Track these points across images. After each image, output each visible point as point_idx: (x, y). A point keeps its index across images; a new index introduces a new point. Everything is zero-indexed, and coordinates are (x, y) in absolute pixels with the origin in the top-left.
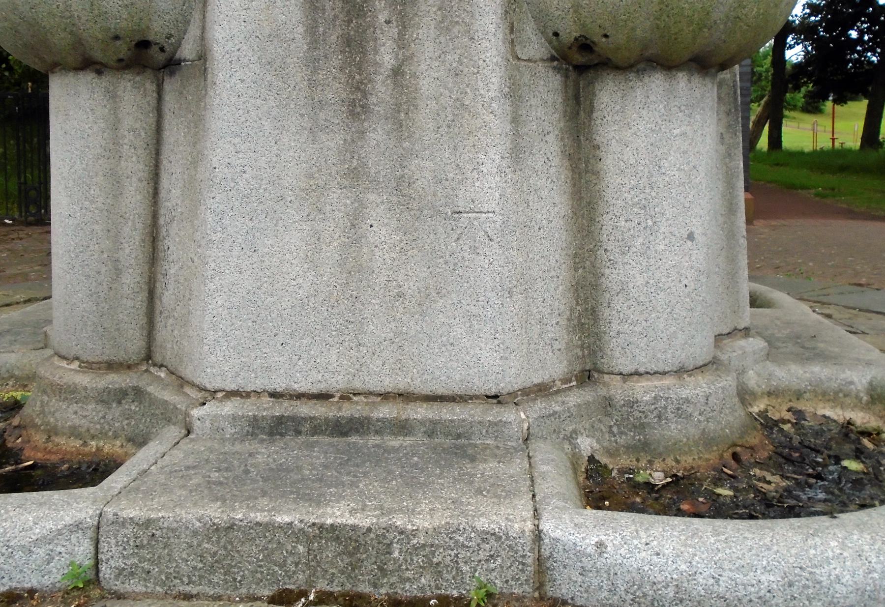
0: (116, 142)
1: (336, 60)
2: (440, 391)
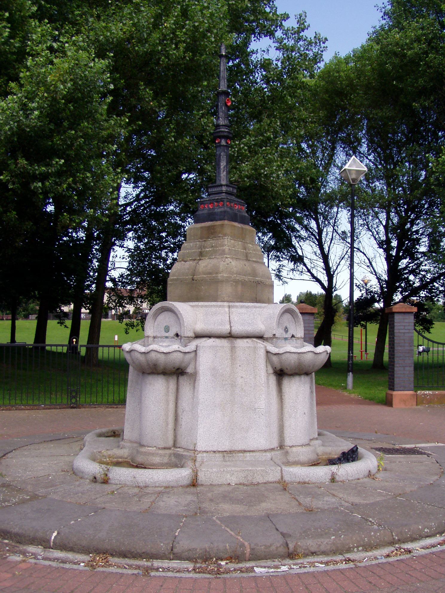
0: (168, 392)
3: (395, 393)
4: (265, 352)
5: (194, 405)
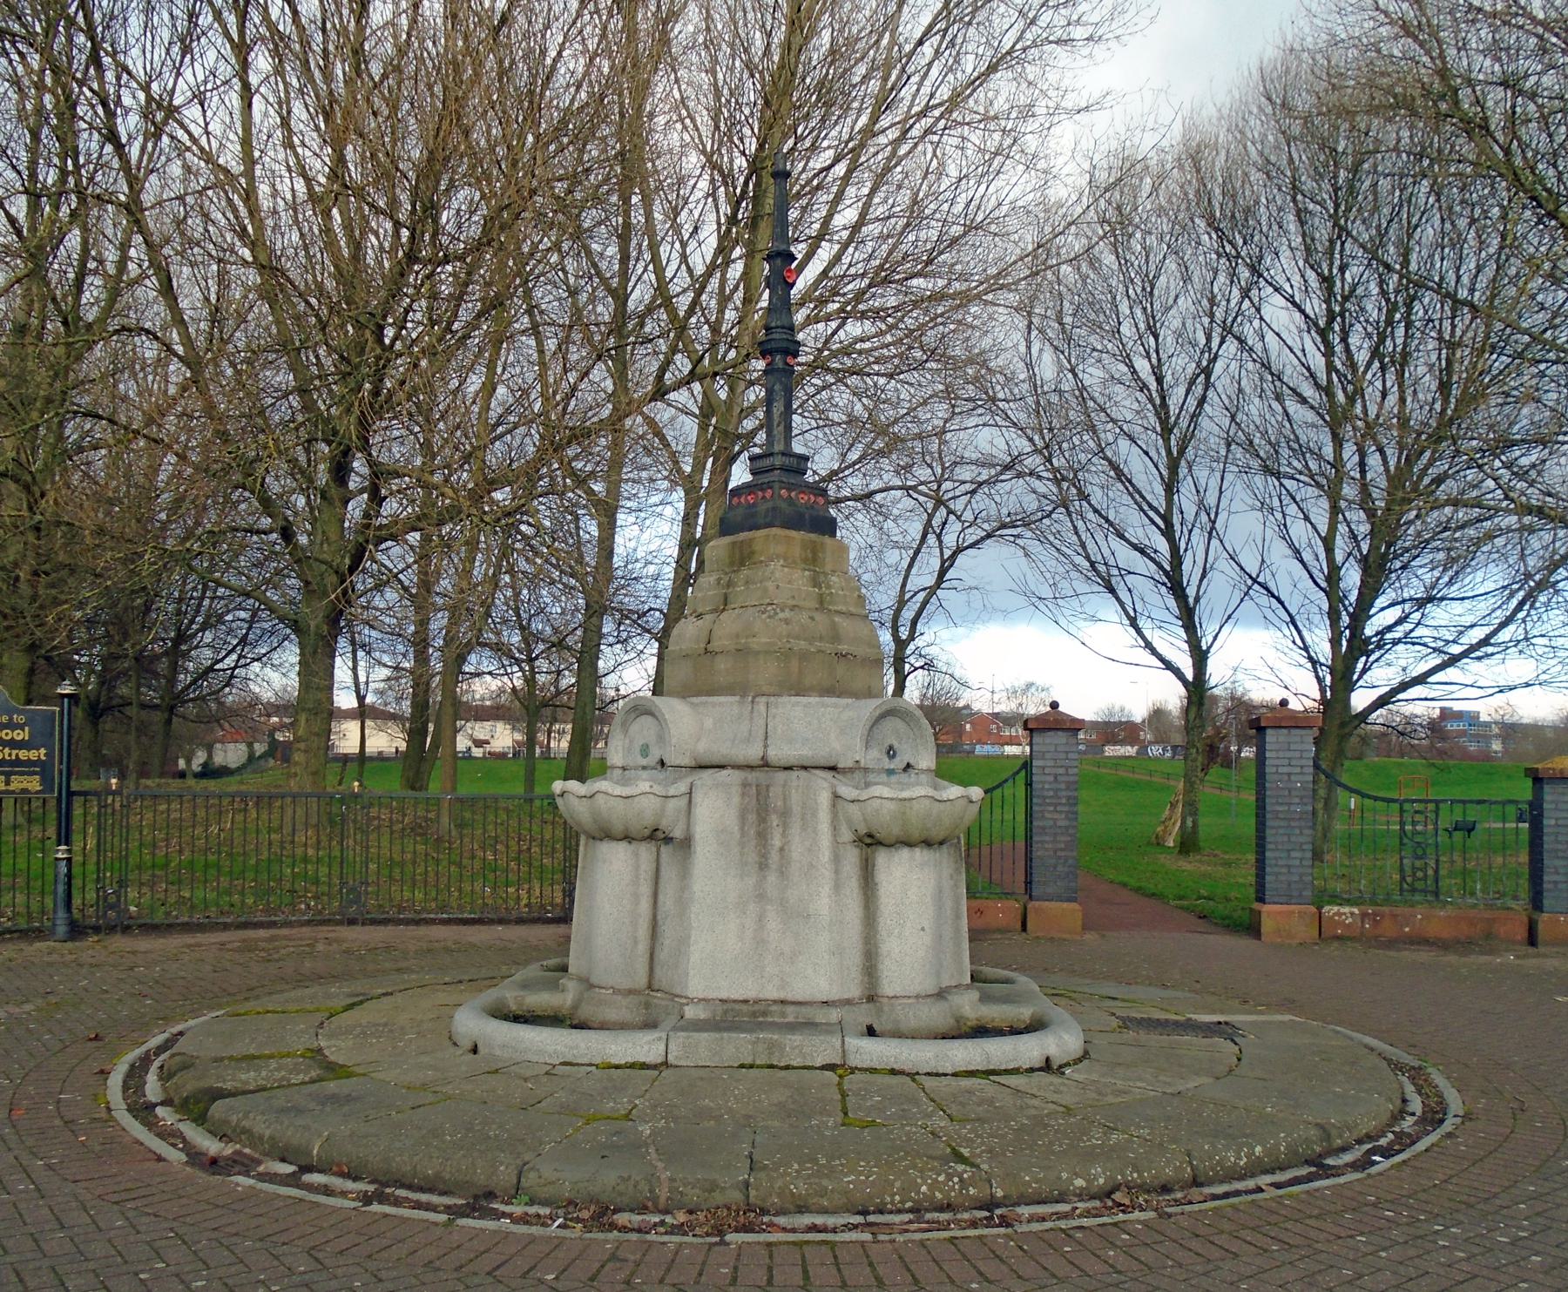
3: (1266, 908)
5: (683, 903)
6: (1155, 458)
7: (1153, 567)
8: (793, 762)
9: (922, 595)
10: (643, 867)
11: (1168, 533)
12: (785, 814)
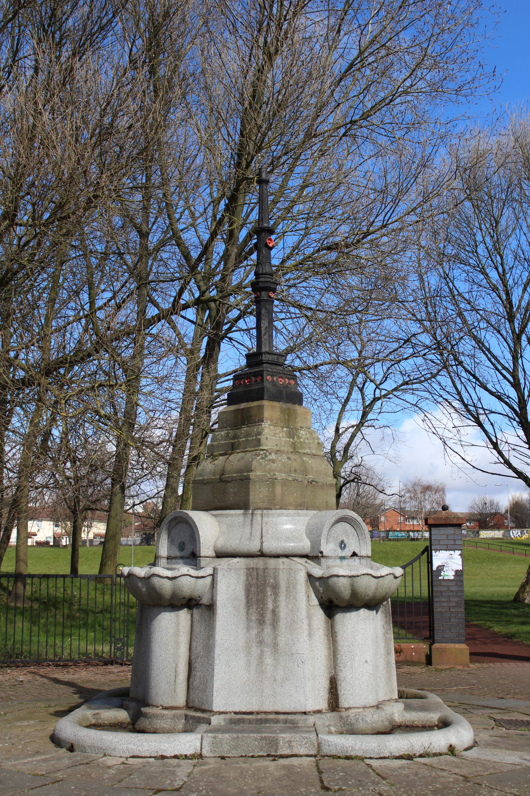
1: (255, 607)
2: (288, 711)
4: (305, 575)
6: (505, 334)
7: (507, 408)
8: (281, 552)
9: (351, 430)
10: (182, 624)
11: (516, 385)
12: (275, 588)
